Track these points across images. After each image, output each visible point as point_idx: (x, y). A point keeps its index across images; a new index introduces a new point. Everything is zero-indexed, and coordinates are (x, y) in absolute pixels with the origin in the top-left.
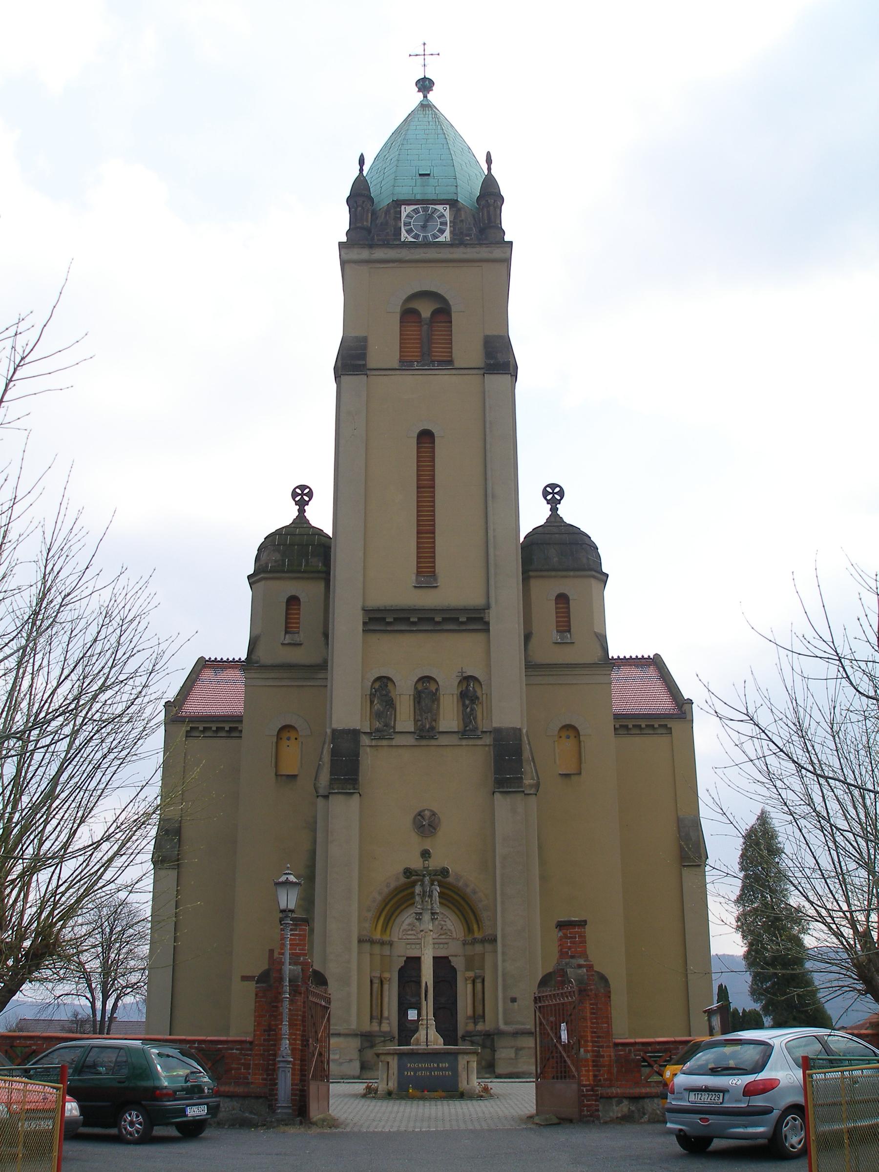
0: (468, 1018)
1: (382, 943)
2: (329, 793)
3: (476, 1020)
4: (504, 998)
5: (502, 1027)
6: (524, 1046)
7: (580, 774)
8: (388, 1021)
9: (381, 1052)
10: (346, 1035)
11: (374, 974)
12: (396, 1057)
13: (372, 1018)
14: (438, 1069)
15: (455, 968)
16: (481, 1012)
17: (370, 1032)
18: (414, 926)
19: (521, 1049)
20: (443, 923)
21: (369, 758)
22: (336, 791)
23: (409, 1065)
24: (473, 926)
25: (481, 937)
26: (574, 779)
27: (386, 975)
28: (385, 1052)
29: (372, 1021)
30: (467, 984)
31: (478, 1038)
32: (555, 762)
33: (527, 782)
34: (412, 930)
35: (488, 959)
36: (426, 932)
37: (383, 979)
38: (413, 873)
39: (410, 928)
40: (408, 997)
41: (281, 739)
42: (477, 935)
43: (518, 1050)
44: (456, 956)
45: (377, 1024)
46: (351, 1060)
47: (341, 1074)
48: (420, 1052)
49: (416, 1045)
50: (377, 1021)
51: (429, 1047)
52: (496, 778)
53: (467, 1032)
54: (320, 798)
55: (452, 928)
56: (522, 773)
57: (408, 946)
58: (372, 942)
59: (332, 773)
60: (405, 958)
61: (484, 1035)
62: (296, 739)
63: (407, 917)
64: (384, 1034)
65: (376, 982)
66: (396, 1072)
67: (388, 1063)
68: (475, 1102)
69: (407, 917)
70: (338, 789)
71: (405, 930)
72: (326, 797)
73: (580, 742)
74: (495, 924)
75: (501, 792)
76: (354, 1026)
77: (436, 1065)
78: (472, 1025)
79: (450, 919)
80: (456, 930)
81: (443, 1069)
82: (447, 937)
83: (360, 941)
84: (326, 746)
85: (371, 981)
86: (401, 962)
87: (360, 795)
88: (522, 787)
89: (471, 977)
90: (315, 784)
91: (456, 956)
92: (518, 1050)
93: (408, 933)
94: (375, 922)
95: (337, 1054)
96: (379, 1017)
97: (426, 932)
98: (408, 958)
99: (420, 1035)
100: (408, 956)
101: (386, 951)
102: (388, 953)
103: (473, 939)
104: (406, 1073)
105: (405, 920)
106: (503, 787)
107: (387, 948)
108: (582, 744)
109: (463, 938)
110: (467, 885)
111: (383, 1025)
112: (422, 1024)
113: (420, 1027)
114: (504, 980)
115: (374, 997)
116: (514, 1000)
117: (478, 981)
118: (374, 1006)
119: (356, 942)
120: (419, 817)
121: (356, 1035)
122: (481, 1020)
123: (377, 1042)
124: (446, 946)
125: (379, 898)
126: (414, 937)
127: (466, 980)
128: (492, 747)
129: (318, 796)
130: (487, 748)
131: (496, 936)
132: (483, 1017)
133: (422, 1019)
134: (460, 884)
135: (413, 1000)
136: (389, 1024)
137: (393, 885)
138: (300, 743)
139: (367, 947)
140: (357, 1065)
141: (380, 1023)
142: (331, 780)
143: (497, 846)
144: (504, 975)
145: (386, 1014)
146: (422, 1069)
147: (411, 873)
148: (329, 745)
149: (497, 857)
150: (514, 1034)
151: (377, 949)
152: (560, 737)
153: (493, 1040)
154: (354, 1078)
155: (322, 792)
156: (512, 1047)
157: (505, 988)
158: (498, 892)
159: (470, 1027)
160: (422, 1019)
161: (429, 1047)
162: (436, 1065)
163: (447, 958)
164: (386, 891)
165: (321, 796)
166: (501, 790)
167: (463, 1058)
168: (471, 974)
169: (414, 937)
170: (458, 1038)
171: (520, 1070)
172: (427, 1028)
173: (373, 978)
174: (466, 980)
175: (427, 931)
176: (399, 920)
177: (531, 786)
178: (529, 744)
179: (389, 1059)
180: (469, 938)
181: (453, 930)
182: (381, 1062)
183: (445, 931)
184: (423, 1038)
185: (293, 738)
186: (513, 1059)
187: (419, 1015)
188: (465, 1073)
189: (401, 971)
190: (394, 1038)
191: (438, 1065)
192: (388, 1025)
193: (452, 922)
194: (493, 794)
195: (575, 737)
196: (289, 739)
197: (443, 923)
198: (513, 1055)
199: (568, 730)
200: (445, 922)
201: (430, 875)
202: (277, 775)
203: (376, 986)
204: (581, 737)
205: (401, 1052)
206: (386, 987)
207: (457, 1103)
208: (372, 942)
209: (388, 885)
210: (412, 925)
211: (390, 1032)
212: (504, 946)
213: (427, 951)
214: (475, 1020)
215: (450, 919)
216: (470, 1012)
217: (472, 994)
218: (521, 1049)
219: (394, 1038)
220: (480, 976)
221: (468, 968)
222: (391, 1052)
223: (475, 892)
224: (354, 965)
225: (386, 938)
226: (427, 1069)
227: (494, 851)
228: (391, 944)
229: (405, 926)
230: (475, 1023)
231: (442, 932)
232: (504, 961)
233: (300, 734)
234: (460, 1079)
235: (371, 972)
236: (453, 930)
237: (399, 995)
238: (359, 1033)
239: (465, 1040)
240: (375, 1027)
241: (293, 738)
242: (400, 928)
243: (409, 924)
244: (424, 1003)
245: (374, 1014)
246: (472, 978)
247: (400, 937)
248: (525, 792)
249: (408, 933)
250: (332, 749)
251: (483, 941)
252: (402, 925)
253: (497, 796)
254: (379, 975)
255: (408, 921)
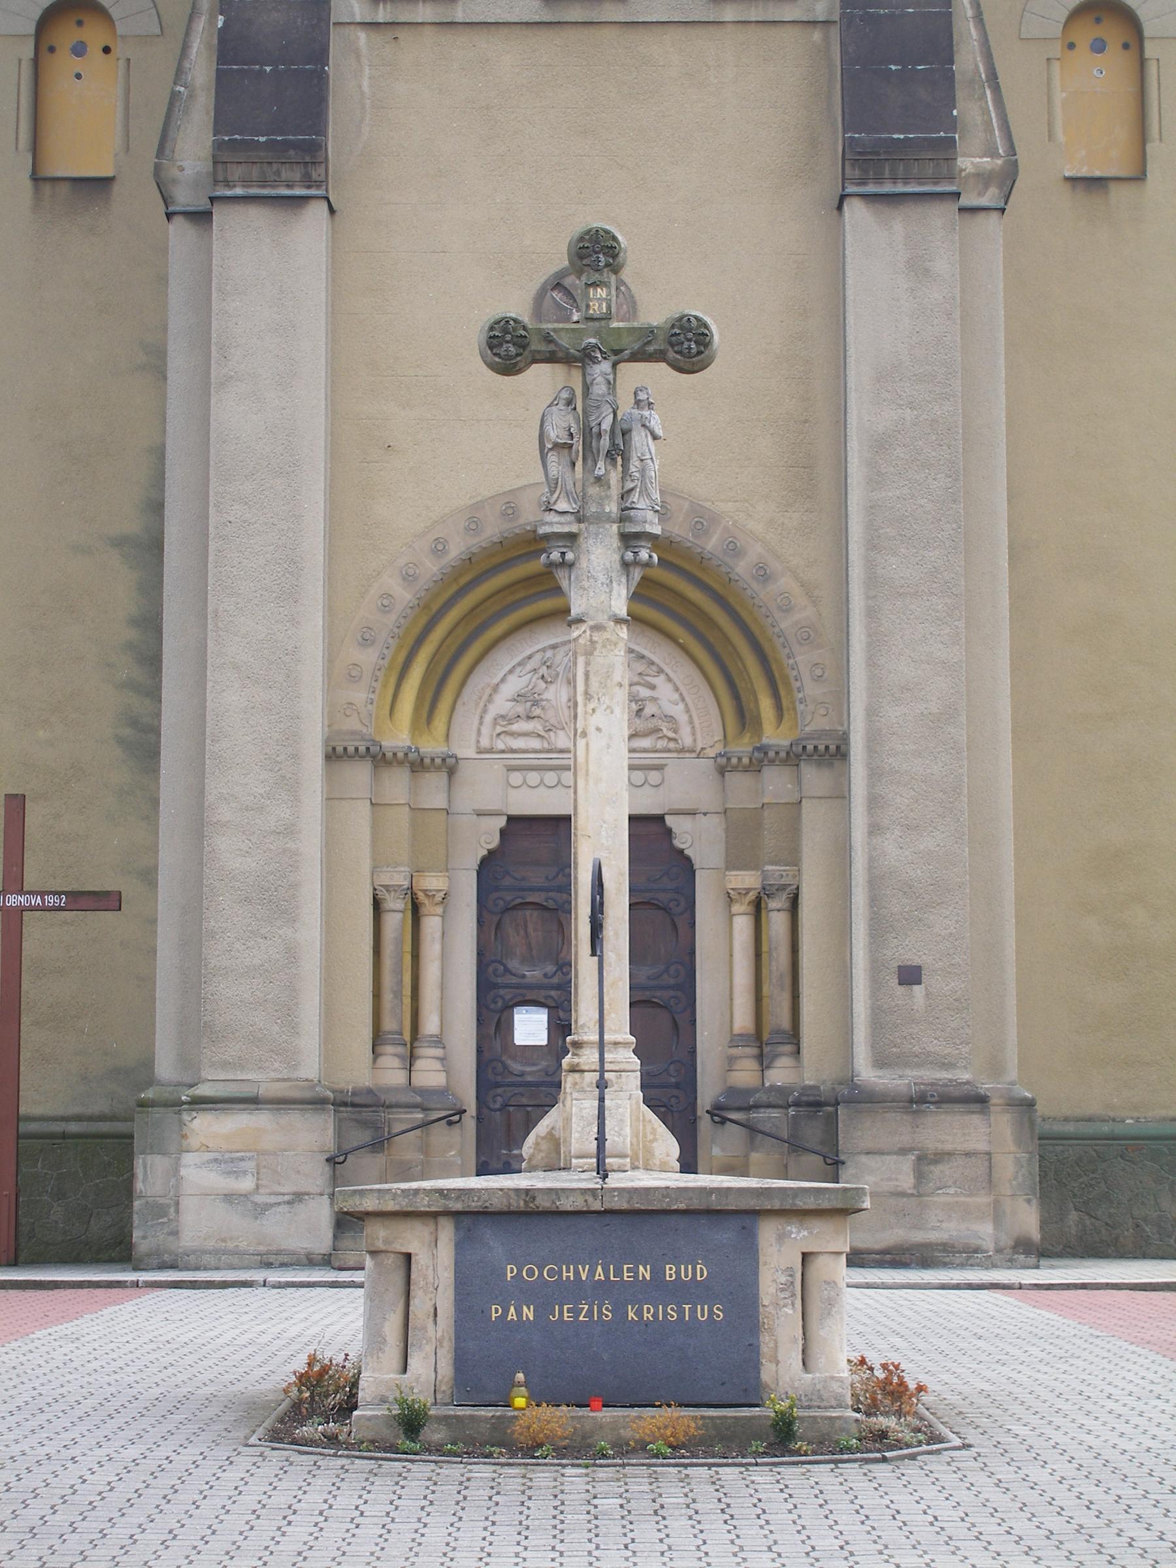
0: (736, 1040)
1: (418, 765)
2: (212, 199)
3: (766, 1049)
4: (876, 968)
5: (867, 1073)
6: (949, 1147)
7: (1140, 177)
8: (438, 1052)
9: (369, 1204)
10: (281, 1103)
11: (385, 879)
12: (447, 1232)
13: (378, 1038)
14: (659, 1290)
15: (688, 859)
16: (785, 1023)
17: (370, 1091)
18: (536, 703)
19: (940, 1157)
20: (644, 692)
21: (367, 71)
22: (239, 191)
23: (510, 1271)
24: (756, 701)
25: (786, 743)
26: (1119, 194)
27: (433, 882)
28: (391, 1206)
29: (380, 1049)
30: (731, 916)
31: (775, 1113)
32: (1051, 136)
33: (967, 163)
34: (530, 718)
35: (815, 818)
36: (598, 628)
37: (421, 895)
38: (536, 345)
39: (520, 709)
40: (514, 964)
41: (52, 50)
42: (775, 735)
43: (926, 1160)
44: (692, 813)
45: (396, 1063)
46: (298, 1197)
47: (262, 1248)
48: (566, 1204)
49: (549, 1168)
50: (400, 1050)
51: (614, 1180)
52: (849, 144)
53: (732, 1091)
54: (178, 221)
55: (678, 711)
56: (953, 125)
57: (516, 778)
58: (379, 759)
59: (220, 123)
60: (502, 822)
61: (797, 1104)
62: (107, 50)
63: (511, 672)
64: (424, 1099)
65: (396, 905)
66: (446, 1302)
67: (408, 1257)
68: (852, 1471)
69: (511, 672)
70: (246, 182)
71: (503, 717)
72: (201, 217)
73: (1142, 62)
74: (842, 695)
75: (871, 198)
76: (310, 1069)
77: (644, 1272)
78: (752, 1064)
79: (669, 680)
80: (691, 722)
81: (681, 1292)
82: (661, 744)
83: (333, 756)
84: (200, 24)
85: (377, 904)
86: (488, 835)
87: (332, 211)
88: (951, 178)
89: (748, 890)
90: (157, 169)
91: (692, 813)
92: (926, 1160)
93: (515, 727)
94: (393, 680)
95: (245, 1173)
96: (407, 1036)
97: (598, 628)
98: (511, 819)
99: (568, 1120)
100: (515, 811)
101: (433, 792)
102: (439, 801)
103: (758, 749)
104: (495, 1312)
105: (503, 680)
106: (879, 180)
107: (435, 782)
108: (1152, 69)
109: (719, 748)
110: (735, 550)
111: (419, 1064)
112: (574, 1069)
113: (568, 1081)
114: (874, 901)
115: (388, 963)
116: (910, 976)
117: (773, 904)
118: (388, 997)
119: (319, 759)
120: (557, 295)
121: (317, 1103)
122: (788, 1048)
123: (397, 1128)
124: (654, 777)
125: (404, 596)
126: (535, 743)
127: (730, 900)
128: (835, 32)
129: (169, 216)
130: (817, 35)
131: (845, 738)
132: (794, 1036)
133: (577, 1045)
134: (712, 544)
135: (533, 974)
136: (442, 1059)
137: (457, 549)
138: (122, 63)
139: (359, 774)
140: (321, 1214)
141: (411, 1059)
142: (219, 146)
143: (853, 397)
144: (874, 883)
145: (431, 1024)
146: (576, 1291)
147: (522, 343)
148: (212, 20)
149: (854, 445)
150: (911, 1101)
151: (397, 785)
152: (1071, 46)
153: (832, 1120)
154: (311, 1262)
155: (184, 198)
156: (903, 1151)
157: (879, 929)
158: (856, 572)
159: (745, 1075)
160: (577, 1045)
161: (614, 1180)
162: (644, 1272)
163: (660, 819)
164: (431, 568)
165: (185, 214)
166: (871, 188)
167: (781, 1238)
168: (747, 880)
169: (535, 743)
170: (699, 1113)
171: (933, 1236)
172: (602, 1085)
173: (383, 893)
174: (730, 900)
175: (602, 619)
176: (481, 680)
177: (984, 179)
178: (979, 18)
179: (413, 1238)
180: (743, 747)
181: (682, 718)
182: (374, 1253)
183: (651, 724)
184: (582, 1139)
185: (95, 50)
186: (903, 1194)
187: (561, 1027)
188: (792, 1313)
189: (488, 867)
190: (462, 1112)
191: (658, 1273)
192: (437, 1065)
193: (677, 689)
194: (840, 208)
195: (1126, 46)
196: (79, 50)
197: (644, 692)
198: (907, 1182)
199: (1098, 20)
200: (653, 687)
201: (616, 352)
202: (37, 178)
203: (395, 921)
204: (1148, 45)
205: (474, 1205)
206: (431, 925)
207: (762, 1477)
208: (379, 759)
209: (438, 548)
210: (530, 701)
211: (443, 1092)
212: (875, 774)
213: (597, 719)
214: (761, 1047)
215: (669, 680)
216: (743, 1020)
217: (751, 951)
218: (940, 1157)
219: (462, 1112)
220: (782, 888)
221: (734, 862)
222: (423, 1204)
223: (764, 575)
224: (311, 844)
225: (431, 746)
226: (603, 1289)
227: (841, 423)
228: (450, 767)
229: (501, 704)
230: (764, 1061)
231: (640, 725)
232: (874, 829)
233: (121, 29)
234: (766, 1342)
235: (374, 870)
236: (682, 718)
237: (480, 954)
238: (331, 1095)
239: (724, 1121)
240: (392, 1074)
241: (95, 50)
242: (485, 711)
243: (519, 698)
244: (585, 965)
245: (389, 1024)
246: (752, 896)
247: (485, 742)
248: (965, 201)
249: (515, 727)
250: (223, 32)
251: (793, 757)
252: (490, 699)
253: (855, 211)
254: (406, 884)
255: (514, 685)
